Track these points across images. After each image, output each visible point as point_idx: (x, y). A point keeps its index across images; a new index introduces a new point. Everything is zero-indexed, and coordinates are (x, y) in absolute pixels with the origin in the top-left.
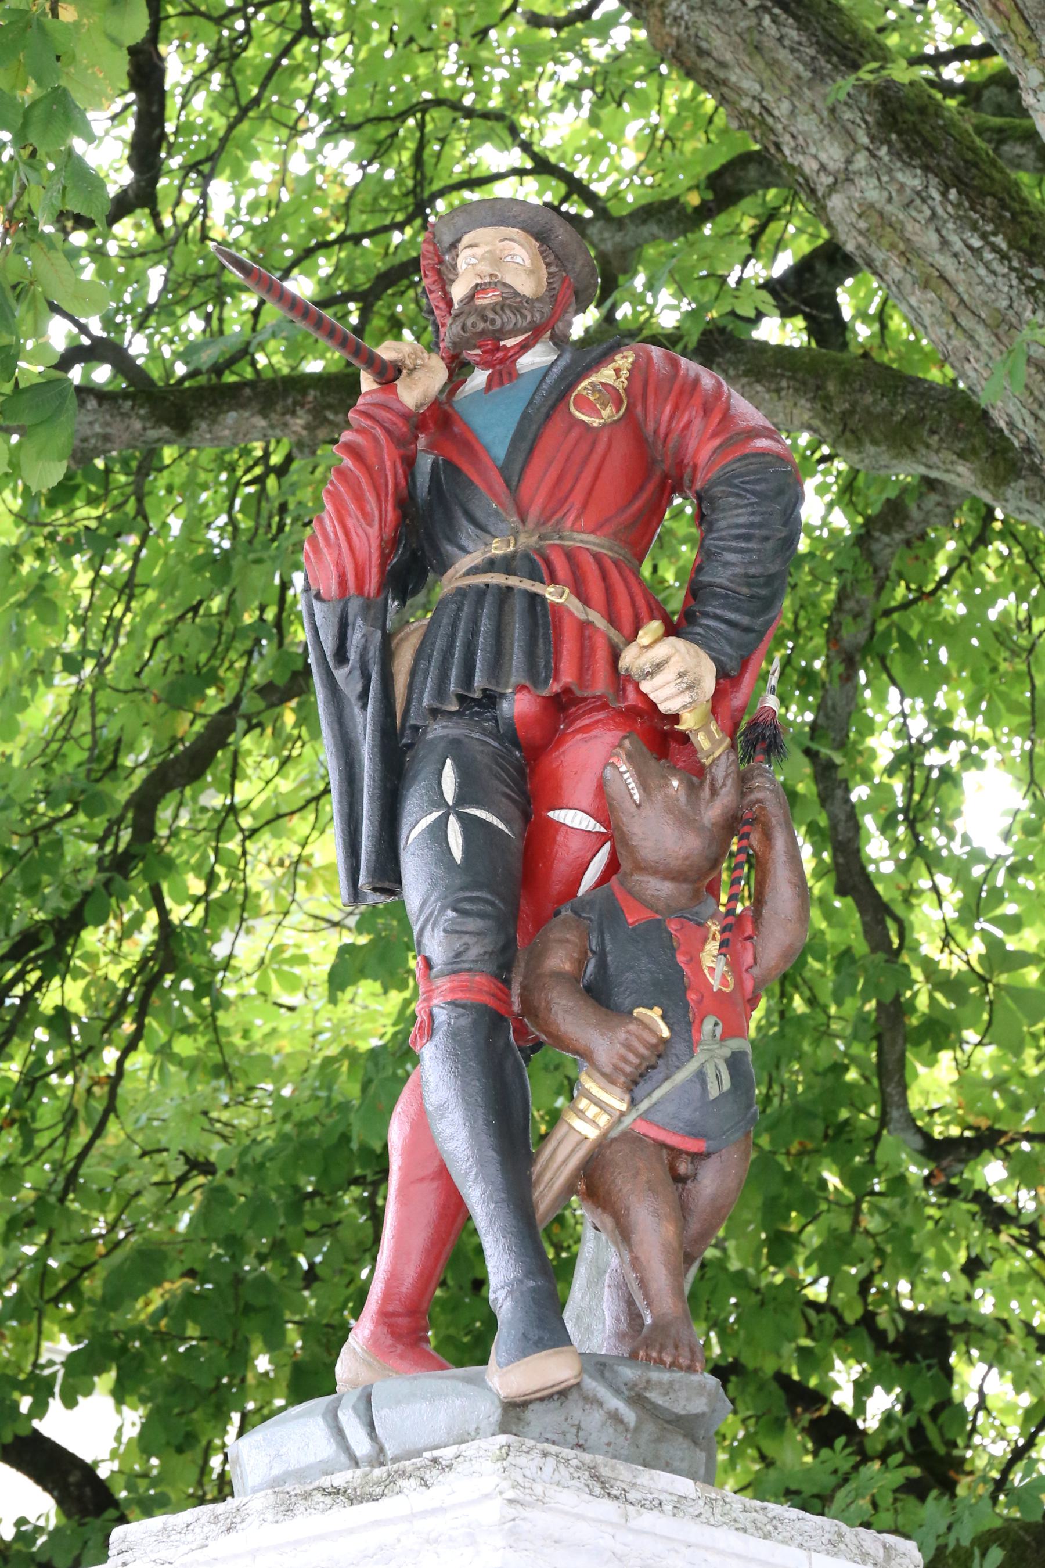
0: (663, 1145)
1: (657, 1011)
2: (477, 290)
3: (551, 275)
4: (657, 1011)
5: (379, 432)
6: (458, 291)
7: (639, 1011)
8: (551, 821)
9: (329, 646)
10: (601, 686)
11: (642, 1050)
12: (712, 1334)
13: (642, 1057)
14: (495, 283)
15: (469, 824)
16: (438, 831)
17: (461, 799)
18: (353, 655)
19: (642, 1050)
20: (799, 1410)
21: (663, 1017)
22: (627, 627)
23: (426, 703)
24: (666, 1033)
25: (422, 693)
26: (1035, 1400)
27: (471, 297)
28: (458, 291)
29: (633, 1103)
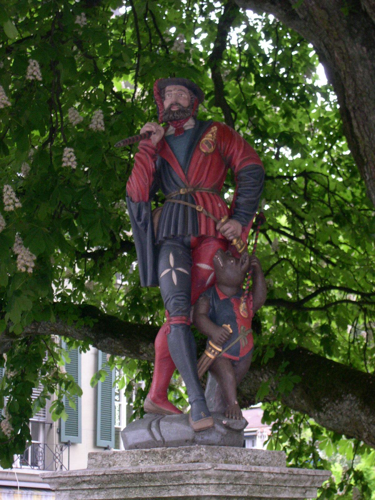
0: (230, 359)
1: (229, 325)
2: (171, 105)
3: (191, 98)
4: (229, 325)
5: (147, 155)
6: (167, 104)
7: (224, 325)
8: (198, 267)
9: (135, 216)
10: (212, 233)
11: (226, 336)
12: (213, 97)
13: (225, 338)
14: (177, 104)
15: (178, 273)
16: (170, 274)
17: (176, 265)
18: (143, 218)
19: (226, 336)
20: (150, 323)
21: (230, 327)
22: (218, 216)
23: (164, 235)
24: (231, 331)
25: (163, 233)
26: (242, 410)
27: (170, 108)
28: (167, 104)
29: (223, 349)
